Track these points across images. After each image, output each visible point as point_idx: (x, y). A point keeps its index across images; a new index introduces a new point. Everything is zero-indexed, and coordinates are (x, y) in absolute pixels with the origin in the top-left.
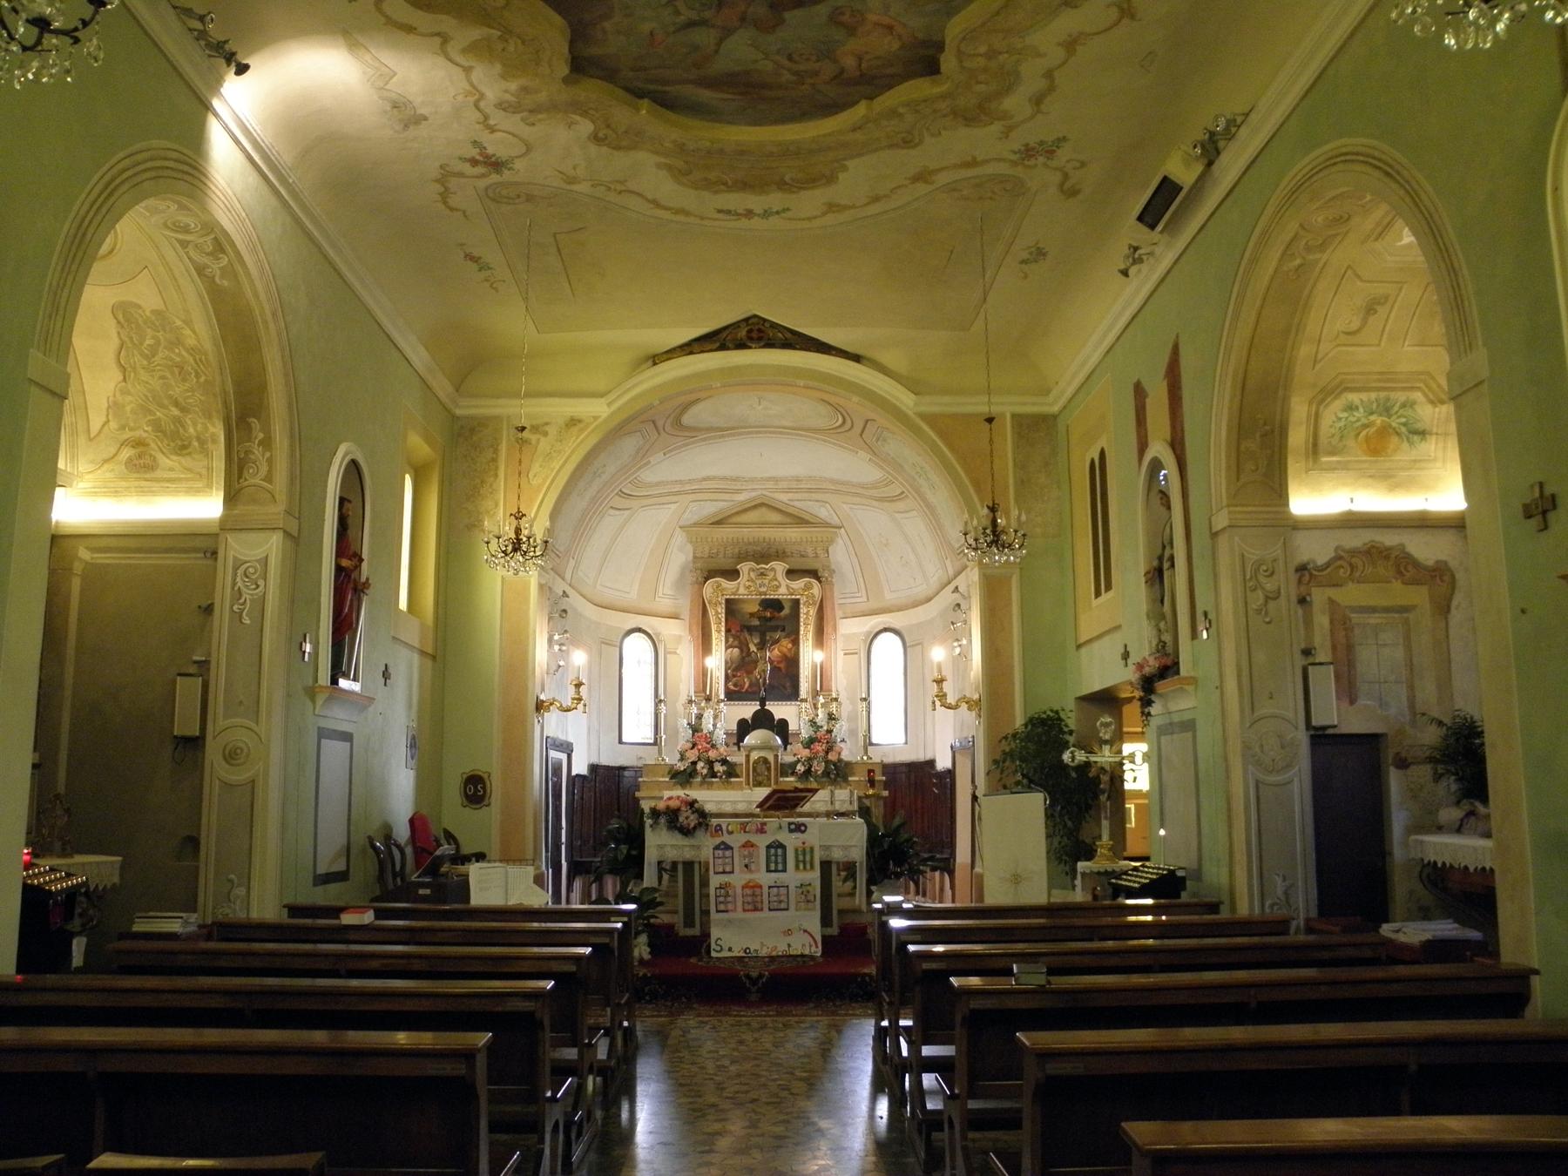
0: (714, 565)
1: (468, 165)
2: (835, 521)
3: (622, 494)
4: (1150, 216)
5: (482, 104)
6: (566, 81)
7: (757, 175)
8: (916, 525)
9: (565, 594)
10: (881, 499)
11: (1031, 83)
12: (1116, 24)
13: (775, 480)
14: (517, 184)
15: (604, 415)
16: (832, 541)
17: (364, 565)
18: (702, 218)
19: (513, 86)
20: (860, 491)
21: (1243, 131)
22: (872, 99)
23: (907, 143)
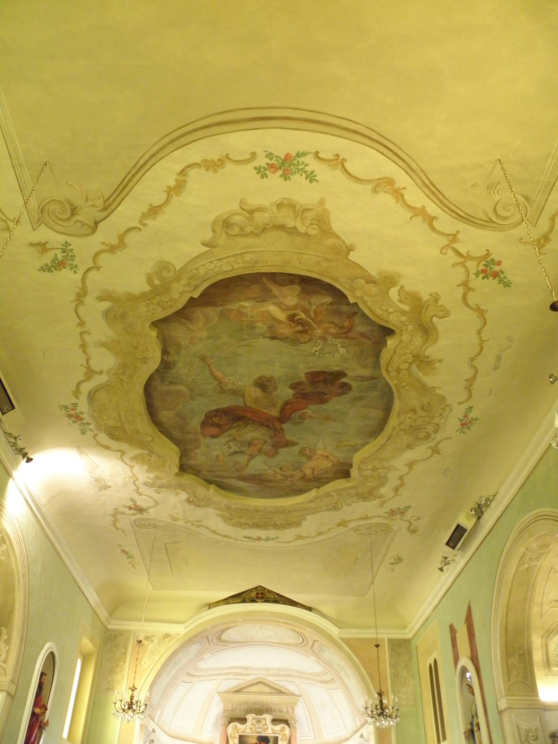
0: (233, 716)
1: (127, 509)
2: (298, 693)
3: (189, 674)
4: (452, 542)
5: (137, 482)
6: (177, 475)
7: (263, 521)
8: (339, 696)
9: (154, 731)
10: (322, 682)
11: (393, 481)
12: (432, 456)
13: (268, 669)
14: (150, 519)
15: (183, 633)
16: (295, 704)
17: (48, 712)
18: (236, 540)
19: (152, 475)
20: (311, 677)
21: (493, 504)
22: (318, 488)
23: (335, 508)
